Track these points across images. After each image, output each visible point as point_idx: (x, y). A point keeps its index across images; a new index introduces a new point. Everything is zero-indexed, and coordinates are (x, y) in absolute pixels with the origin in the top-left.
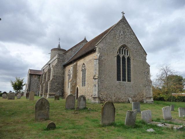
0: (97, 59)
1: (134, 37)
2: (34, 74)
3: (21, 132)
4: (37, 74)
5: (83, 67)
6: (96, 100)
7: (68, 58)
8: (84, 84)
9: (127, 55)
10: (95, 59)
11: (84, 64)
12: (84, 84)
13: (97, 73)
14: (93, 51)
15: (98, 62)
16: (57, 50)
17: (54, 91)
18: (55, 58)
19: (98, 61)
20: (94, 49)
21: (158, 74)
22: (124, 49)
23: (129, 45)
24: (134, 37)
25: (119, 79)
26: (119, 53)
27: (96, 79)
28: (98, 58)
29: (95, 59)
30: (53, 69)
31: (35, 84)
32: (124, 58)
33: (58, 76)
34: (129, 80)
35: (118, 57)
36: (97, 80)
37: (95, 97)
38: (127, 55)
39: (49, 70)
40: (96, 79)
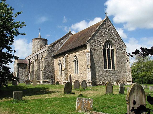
0: (89, 53)
1: (116, 33)
2: (21, 64)
3: (80, 112)
4: (24, 63)
5: (75, 58)
6: (90, 84)
7: (56, 50)
8: (77, 71)
9: (111, 48)
10: (87, 53)
11: (76, 56)
12: (77, 71)
13: (90, 64)
14: (84, 47)
15: (89, 55)
16: (39, 40)
17: (47, 79)
18: (45, 50)
19: (90, 54)
20: (85, 44)
21: (85, 22)
22: (109, 43)
23: (112, 40)
24: (116, 33)
25: (105, 68)
26: (105, 47)
27: (89, 68)
28: (89, 52)
29: (87, 53)
30: (44, 59)
31: (22, 72)
32: (109, 50)
33: (49, 65)
34: (113, 68)
35: (104, 50)
36: (90, 69)
37: (90, 81)
38: (111, 48)
39: (38, 60)
40: (89, 68)
